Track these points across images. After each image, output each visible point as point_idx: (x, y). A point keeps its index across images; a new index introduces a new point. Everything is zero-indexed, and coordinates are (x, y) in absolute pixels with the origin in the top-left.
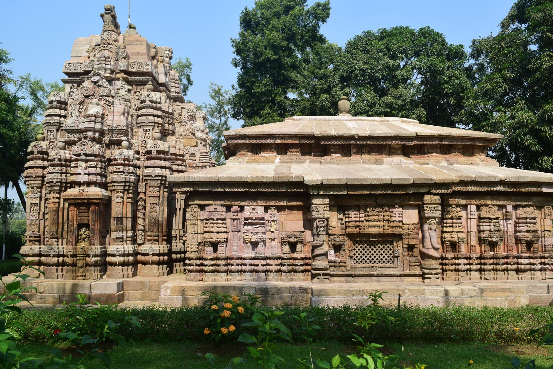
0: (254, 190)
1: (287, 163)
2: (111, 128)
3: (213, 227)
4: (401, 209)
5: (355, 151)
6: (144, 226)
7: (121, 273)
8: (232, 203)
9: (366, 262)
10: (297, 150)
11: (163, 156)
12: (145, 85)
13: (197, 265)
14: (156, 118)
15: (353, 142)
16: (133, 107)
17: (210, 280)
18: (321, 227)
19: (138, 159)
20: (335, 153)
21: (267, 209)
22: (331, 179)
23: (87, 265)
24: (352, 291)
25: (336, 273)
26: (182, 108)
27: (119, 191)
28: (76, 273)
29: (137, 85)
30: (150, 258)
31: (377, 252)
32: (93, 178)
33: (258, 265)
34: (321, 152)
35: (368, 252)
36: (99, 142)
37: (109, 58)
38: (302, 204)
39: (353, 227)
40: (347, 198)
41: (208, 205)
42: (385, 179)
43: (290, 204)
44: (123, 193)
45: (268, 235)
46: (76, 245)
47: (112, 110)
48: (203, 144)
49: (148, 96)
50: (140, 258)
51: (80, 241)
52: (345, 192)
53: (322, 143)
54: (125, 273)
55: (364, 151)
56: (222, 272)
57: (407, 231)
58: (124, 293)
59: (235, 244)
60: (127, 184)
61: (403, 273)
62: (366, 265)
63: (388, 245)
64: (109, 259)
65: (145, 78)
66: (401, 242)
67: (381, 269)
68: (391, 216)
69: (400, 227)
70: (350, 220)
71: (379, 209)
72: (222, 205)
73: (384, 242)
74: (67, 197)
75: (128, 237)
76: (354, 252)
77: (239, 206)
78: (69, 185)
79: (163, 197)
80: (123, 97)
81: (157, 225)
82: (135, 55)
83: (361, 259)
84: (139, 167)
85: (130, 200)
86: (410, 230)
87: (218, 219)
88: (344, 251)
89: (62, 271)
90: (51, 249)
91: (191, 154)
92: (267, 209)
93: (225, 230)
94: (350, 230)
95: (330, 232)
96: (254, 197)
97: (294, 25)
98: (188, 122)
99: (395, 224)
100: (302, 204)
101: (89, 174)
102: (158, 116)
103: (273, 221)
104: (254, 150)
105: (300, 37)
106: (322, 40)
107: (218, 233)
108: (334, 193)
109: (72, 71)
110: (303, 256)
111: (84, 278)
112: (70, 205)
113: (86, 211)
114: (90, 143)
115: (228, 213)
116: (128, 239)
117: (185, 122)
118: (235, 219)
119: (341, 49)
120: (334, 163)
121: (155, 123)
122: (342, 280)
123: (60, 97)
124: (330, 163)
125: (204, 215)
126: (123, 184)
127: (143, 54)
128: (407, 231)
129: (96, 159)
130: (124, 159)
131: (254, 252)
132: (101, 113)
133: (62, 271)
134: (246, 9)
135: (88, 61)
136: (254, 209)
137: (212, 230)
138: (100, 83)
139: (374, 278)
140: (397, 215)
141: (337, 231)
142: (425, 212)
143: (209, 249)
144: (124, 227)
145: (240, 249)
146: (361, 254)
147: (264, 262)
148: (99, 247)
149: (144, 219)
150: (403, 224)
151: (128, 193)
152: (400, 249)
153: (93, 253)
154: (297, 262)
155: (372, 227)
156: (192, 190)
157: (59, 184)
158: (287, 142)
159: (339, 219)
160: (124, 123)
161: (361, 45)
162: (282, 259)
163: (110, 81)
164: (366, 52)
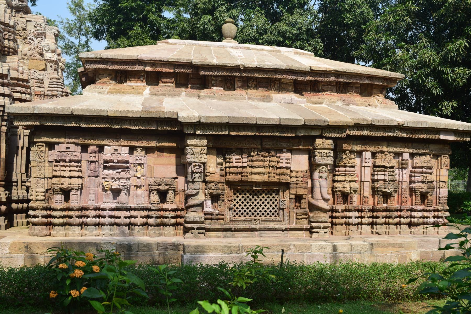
0: (117, 127)
4: (289, 154)
8: (89, 142)
10: (170, 81)
13: (43, 217)
15: (238, 74)
17: (60, 235)
18: (197, 173)
20: (216, 86)
21: (132, 150)
22: (210, 117)
24: (230, 247)
26: (27, 21)
33: (119, 217)
34: (200, 85)
38: (175, 145)
39: (234, 173)
40: (228, 139)
41: (58, 143)
42: (273, 119)
45: (133, 181)
48: (53, 67)
52: (226, 133)
53: (202, 73)
55: (250, 85)
56: (75, 225)
57: (295, 179)
59: (91, 192)
61: (288, 226)
62: (248, 218)
63: (274, 195)
66: (287, 191)
67: (264, 223)
68: (278, 162)
69: (287, 174)
70: (231, 165)
71: (264, 154)
72: (76, 144)
73: (269, 192)
77: (98, 146)
83: (242, 211)
86: (298, 179)
87: (70, 161)
88: (223, 201)
91: (38, 79)
92: (132, 150)
93: (79, 174)
94: (230, 177)
95: (207, 179)
98: (34, 39)
99: (282, 171)
100: (175, 145)
103: (140, 164)
104: (118, 78)
107: (70, 177)
108: (213, 133)
110: (174, 206)
115: (84, 154)
117: (30, 39)
118: (92, 162)
120: (215, 98)
124: (210, 97)
125: (53, 155)
128: (295, 179)
131: (115, 201)
136: (116, 150)
139: (256, 232)
140: (285, 161)
142: (316, 158)
143: (60, 197)
147: (127, 214)
150: (291, 171)
152: (287, 199)
154: (167, 214)
155: (256, 174)
156: (38, 124)
158: (159, 69)
159: (218, 164)
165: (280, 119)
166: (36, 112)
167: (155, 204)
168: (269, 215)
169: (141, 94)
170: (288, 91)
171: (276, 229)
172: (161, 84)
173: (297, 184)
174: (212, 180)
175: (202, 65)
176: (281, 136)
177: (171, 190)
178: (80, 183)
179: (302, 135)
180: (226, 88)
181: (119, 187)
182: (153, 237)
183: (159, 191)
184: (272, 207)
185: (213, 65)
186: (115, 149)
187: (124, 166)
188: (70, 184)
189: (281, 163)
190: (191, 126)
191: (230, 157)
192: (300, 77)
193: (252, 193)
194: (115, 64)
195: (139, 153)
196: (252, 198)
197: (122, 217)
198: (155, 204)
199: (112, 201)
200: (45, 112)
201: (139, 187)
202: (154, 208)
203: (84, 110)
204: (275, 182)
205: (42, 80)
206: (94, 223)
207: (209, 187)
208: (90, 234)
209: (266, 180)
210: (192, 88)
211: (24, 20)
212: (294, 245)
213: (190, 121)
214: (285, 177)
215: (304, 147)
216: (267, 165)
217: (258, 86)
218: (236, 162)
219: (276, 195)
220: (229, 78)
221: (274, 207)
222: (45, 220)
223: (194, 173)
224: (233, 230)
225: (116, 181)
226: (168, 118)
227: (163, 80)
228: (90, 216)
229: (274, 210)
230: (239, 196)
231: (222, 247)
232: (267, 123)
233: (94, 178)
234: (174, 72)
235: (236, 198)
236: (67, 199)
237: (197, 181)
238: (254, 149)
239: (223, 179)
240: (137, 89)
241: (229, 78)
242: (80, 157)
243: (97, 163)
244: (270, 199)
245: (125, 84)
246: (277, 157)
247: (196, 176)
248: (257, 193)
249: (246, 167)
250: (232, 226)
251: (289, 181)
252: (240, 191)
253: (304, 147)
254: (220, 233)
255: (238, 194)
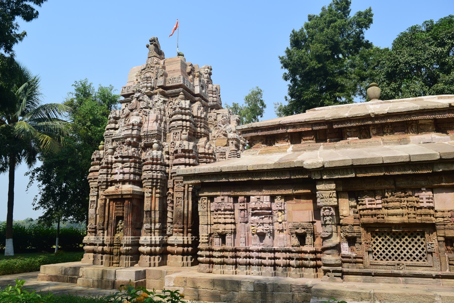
0: (257, 179)
1: (300, 151)
2: (146, 134)
3: (220, 218)
4: (430, 193)
5: (374, 132)
6: (172, 219)
7: (148, 262)
8: (238, 193)
9: (390, 258)
10: (310, 138)
11: (187, 154)
12: (178, 96)
13: (207, 256)
14: (184, 122)
15: (370, 122)
16: (167, 115)
17: (218, 273)
18: (328, 216)
19: (168, 159)
20: (351, 137)
21: (273, 198)
22: (333, 161)
23: (121, 254)
24: (360, 293)
25: (350, 270)
26: (217, 114)
27: (148, 187)
28: (113, 260)
29: (172, 97)
30: (175, 249)
31: (404, 246)
32: (127, 177)
33: (265, 258)
34: (337, 138)
35: (392, 246)
36: (135, 145)
37: (150, 78)
38: (309, 191)
39: (368, 215)
40: (356, 182)
41: (216, 196)
42: (401, 157)
43: (297, 192)
44: (152, 188)
45: (277, 226)
46: (114, 235)
47: (147, 119)
48: (234, 143)
49: (178, 104)
50: (169, 248)
51: (117, 232)
52: (353, 175)
53: (335, 126)
54: (152, 262)
55: (385, 131)
56: (230, 264)
57: (441, 220)
58: (145, 281)
59: (242, 236)
60: (155, 181)
61: (440, 273)
62: (390, 261)
63: (419, 237)
64: (169, 248)
65: (177, 90)
66: (435, 233)
67: (410, 268)
68: (417, 202)
69: (431, 215)
70: (364, 207)
71: (399, 194)
72: (229, 196)
73: (412, 234)
74: (107, 194)
75: (157, 229)
76: (374, 246)
77: (245, 196)
78: (109, 184)
79: (188, 192)
80: (158, 107)
81: (182, 217)
82: (172, 73)
83: (384, 255)
84: (168, 166)
85: (158, 195)
86: (445, 219)
87: (225, 210)
88: (361, 244)
89: (187, 260)
90: (98, 239)
91: (222, 152)
92: (273, 198)
93: (233, 221)
94: (365, 220)
95: (341, 221)
96: (260, 186)
97: (335, 35)
98: (222, 125)
99: (423, 211)
100: (309, 191)
101: (124, 173)
102: (187, 121)
103: (280, 211)
104: (268, 142)
105: (343, 45)
106: (368, 45)
107: (225, 224)
108: (340, 177)
109: (126, 93)
110: (312, 249)
111: (118, 265)
112: (110, 200)
113: (122, 205)
114: (126, 147)
115: (236, 204)
116: (156, 231)
117: (219, 126)
118: (242, 210)
119: (387, 50)
120: (349, 147)
121: (183, 126)
122: (359, 279)
123: (116, 114)
124: (344, 147)
125: (213, 206)
126: (151, 180)
127: (178, 71)
128: (441, 220)
129: (131, 160)
130: (153, 159)
131: (262, 244)
132: (139, 122)
133: (187, 260)
134: (293, 31)
135: (136, 82)
136: (260, 199)
137: (220, 221)
138: (141, 98)
139: (400, 278)
140: (425, 200)
141: (350, 220)
143: (217, 240)
144: (153, 220)
145: (247, 241)
146: (383, 249)
147: (272, 255)
148: (130, 237)
149: (172, 213)
150: (436, 211)
151: (156, 189)
152: (435, 242)
153: (125, 243)
154: (306, 256)
155: (393, 215)
156: (199, 182)
157: (105, 184)
158: (299, 130)
159: (351, 207)
160: (156, 128)
161: (407, 40)
162: (290, 251)
163: (150, 96)
164: (411, 45)
165: (410, 156)
166: (196, 172)
167: (296, 246)
168: (416, 260)
169: (286, 151)
170: (428, 131)
171: (424, 275)
172: (303, 142)
173: (445, 225)
174: (346, 222)
175: (334, 119)
176: (414, 174)
177: (309, 233)
178: (233, 228)
179: (441, 170)
180: (362, 137)
181: (262, 231)
182: (295, 278)
183: (298, 235)
184: (418, 251)
185: (344, 118)
186: (258, 199)
187: (268, 212)
188: (225, 229)
189: (421, 202)
190: (317, 172)
191: (363, 199)
192: (438, 116)
193: (393, 236)
194: (263, 131)
195: (278, 201)
196: (393, 241)
197: (267, 258)
198: (296, 246)
199: (258, 244)
200: (202, 172)
201: (282, 231)
202: (294, 250)
203: (230, 167)
204: (416, 223)
205: (225, 153)
206: (245, 262)
207: (344, 230)
208: (242, 273)
209: (405, 222)
210: (330, 142)
211: (216, 114)
212: (440, 296)
213: (315, 167)
214: (428, 217)
215: (447, 184)
216: (405, 206)
217: (394, 131)
218: (369, 204)
219: (421, 237)
220: (363, 128)
221: (421, 251)
222: (208, 259)
223: (325, 216)
224: (373, 274)
225: (260, 226)
226: (298, 167)
227: (304, 138)
228: (241, 256)
229: (422, 254)
230: (378, 238)
231: (351, 292)
232: (394, 162)
233: (244, 224)
234: (312, 130)
235: (376, 241)
236: (224, 242)
237: (329, 224)
238: (388, 189)
239: (357, 222)
240: (282, 148)
241: (363, 128)
242: (232, 206)
243: (246, 211)
244: (414, 242)
245: (274, 146)
246: (416, 197)
247: (327, 219)
248: (399, 236)
249: (381, 209)
250: (372, 270)
251: (434, 222)
252: (379, 233)
253: (447, 184)
254: (359, 278)
255: (377, 237)
